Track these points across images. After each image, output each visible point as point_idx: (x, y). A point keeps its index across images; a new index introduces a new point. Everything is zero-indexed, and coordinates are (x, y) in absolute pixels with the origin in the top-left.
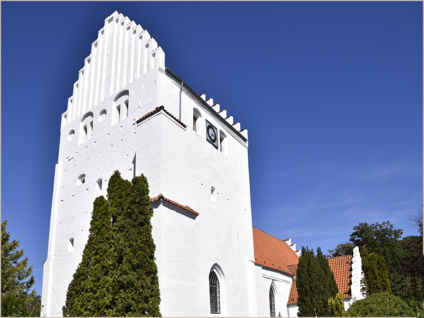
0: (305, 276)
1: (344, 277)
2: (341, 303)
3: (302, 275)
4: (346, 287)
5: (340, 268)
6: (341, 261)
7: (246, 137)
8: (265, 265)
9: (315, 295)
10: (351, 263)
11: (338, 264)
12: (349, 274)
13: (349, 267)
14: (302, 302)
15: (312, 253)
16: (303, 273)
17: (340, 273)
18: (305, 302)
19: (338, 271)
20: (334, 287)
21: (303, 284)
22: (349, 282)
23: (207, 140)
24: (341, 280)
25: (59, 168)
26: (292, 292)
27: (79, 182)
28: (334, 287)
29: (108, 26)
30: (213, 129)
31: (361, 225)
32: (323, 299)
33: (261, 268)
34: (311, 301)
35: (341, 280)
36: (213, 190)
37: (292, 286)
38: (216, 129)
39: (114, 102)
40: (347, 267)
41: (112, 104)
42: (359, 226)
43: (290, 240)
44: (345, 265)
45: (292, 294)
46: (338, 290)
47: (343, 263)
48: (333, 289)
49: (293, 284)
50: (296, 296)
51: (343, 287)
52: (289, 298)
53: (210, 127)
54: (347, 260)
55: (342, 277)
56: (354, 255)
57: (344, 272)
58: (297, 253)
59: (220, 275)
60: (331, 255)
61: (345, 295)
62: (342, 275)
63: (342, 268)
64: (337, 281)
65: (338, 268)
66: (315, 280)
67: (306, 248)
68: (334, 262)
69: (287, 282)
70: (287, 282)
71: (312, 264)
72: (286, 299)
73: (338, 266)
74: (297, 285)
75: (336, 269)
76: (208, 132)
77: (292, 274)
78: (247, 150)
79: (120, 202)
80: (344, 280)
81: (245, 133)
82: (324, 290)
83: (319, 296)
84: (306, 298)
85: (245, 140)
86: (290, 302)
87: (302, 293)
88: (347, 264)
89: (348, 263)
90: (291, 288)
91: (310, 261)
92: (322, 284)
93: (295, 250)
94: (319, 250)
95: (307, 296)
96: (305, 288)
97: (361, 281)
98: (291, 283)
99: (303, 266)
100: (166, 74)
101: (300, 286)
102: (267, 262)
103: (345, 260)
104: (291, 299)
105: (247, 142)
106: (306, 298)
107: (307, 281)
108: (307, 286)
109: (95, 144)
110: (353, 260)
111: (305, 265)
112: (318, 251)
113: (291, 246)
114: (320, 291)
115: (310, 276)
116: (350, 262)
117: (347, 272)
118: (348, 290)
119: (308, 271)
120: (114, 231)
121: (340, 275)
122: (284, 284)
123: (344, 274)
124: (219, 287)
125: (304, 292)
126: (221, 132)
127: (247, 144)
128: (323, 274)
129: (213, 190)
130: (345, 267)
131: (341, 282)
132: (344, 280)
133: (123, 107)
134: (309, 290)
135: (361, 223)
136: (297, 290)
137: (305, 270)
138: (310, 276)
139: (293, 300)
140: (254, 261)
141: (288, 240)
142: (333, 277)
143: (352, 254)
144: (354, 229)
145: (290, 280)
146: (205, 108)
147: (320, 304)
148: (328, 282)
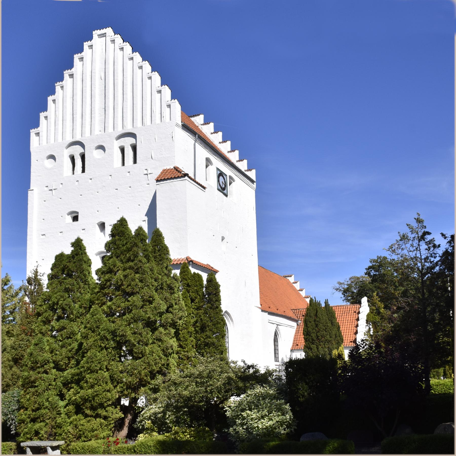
0: (312, 325)
1: (351, 326)
2: (379, 313)
3: (309, 325)
4: (352, 336)
5: (347, 316)
6: (348, 310)
7: (254, 179)
8: (270, 310)
9: (321, 343)
10: (359, 313)
11: (346, 312)
12: (356, 323)
13: (357, 316)
14: (309, 349)
15: (319, 304)
16: (310, 322)
17: (347, 321)
18: (311, 349)
19: (345, 319)
20: (339, 336)
21: (310, 332)
22: (355, 331)
23: (218, 190)
24: (348, 329)
25: (35, 198)
26: (296, 337)
27: (69, 219)
28: (339, 336)
29: (97, 41)
30: (223, 176)
31: (380, 258)
32: (328, 348)
33: (267, 314)
34: (318, 348)
35: (348, 329)
36: (223, 239)
37: (296, 331)
38: (226, 175)
39: (115, 141)
40: (354, 316)
41: (113, 142)
42: (376, 259)
43: (293, 276)
44: (352, 314)
45: (296, 339)
46: (343, 340)
47: (350, 312)
48: (339, 338)
49: (298, 329)
50: (302, 343)
51: (349, 336)
52: (294, 343)
53: (221, 174)
54: (355, 309)
55: (348, 326)
56: (362, 305)
57: (351, 321)
58: (300, 292)
59: (229, 321)
60: (341, 288)
61: (351, 343)
62: (349, 324)
63: (350, 316)
64: (343, 331)
65: (345, 317)
66: (322, 330)
67: (314, 299)
68: (342, 310)
69: (291, 326)
70: (291, 326)
71: (319, 315)
72: (290, 344)
73: (345, 314)
74: (303, 333)
75: (343, 317)
76: (219, 181)
77: (296, 319)
78: (254, 192)
79: (196, 290)
80: (350, 329)
81: (252, 174)
82: (330, 339)
83: (324, 345)
84: (312, 346)
85: (252, 181)
86: (294, 347)
87: (309, 341)
88: (355, 314)
89: (355, 312)
90: (296, 333)
91: (317, 312)
92: (329, 334)
93: (298, 288)
94: (326, 303)
95: (313, 344)
96: (312, 337)
97: (364, 333)
98: (296, 328)
99: (310, 316)
100: (182, 129)
101: (307, 334)
102: (271, 306)
103: (353, 309)
104: (295, 344)
105: (255, 184)
106: (312, 346)
107: (314, 331)
108: (313, 335)
109: (90, 181)
110: (361, 310)
111: (312, 315)
112: (325, 303)
113: (294, 283)
114: (326, 340)
115: (317, 326)
116: (357, 311)
117: (354, 321)
118: (354, 338)
119: (315, 321)
120: (193, 309)
121: (346, 324)
122: (289, 328)
123: (351, 323)
124: (228, 332)
125: (311, 340)
126: (230, 177)
127: (255, 185)
128: (329, 325)
129: (223, 239)
130: (352, 316)
131: (348, 331)
132: (350, 329)
133: (129, 153)
134: (315, 339)
135: (379, 256)
136: (304, 338)
137: (312, 320)
138: (317, 326)
139: (297, 345)
140: (260, 306)
141: (291, 276)
142: (339, 328)
143: (360, 303)
144: (371, 262)
145: (294, 324)
146: (216, 156)
147: (326, 352)
148: (334, 333)
